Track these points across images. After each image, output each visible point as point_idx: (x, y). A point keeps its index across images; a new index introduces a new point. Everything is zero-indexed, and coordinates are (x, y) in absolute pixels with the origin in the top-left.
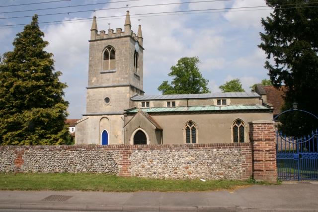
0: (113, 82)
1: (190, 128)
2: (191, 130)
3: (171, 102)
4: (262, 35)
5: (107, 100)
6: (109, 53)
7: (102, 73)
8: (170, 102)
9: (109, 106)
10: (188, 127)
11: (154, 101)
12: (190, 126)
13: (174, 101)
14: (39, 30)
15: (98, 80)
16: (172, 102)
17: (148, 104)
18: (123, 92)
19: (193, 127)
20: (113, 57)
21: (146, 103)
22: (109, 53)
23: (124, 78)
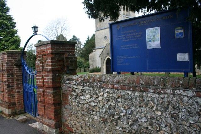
14: (77, 38)
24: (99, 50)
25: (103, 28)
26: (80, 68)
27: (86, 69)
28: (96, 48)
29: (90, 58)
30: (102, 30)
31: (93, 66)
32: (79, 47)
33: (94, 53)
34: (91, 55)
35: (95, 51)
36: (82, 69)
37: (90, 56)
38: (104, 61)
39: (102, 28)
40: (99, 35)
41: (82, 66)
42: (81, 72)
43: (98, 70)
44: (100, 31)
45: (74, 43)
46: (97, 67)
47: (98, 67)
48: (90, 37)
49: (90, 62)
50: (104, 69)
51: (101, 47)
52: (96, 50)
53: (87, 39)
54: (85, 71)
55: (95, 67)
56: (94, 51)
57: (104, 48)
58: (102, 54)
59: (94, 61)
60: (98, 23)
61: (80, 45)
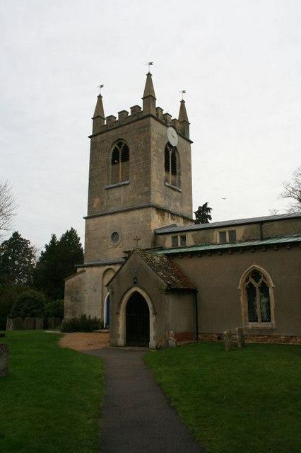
0: (125, 202)
1: (256, 285)
2: (258, 291)
3: (227, 230)
4: (54, 237)
5: (115, 235)
6: (120, 152)
7: (108, 189)
8: (225, 233)
9: (118, 248)
10: (251, 284)
11: (192, 233)
12: (257, 281)
13: (233, 229)
14: (22, 239)
15: (102, 203)
16: (230, 232)
17: (184, 238)
18: (141, 219)
19: (263, 283)
20: (126, 157)
21: (227, 234)
22: (120, 152)
23: (142, 194)
24: (94, 269)
25: (110, 211)
26: (34, 315)
27: (51, 320)
28: (85, 264)
29: (66, 289)
30: (106, 217)
31: (74, 313)
32: (25, 262)
33: (80, 276)
34: (69, 282)
35: (83, 271)
36: (39, 321)
37: (66, 283)
38: (120, 302)
39: (106, 212)
40: (95, 229)
41: (39, 310)
42: (35, 328)
43: (87, 326)
44: (102, 218)
45: (71, 236)
46: (84, 317)
47: (88, 317)
48: (58, 239)
49: (67, 301)
50: (119, 326)
51: (100, 263)
52: (85, 269)
53: (48, 242)
54: (46, 326)
55: (78, 316)
56: (79, 270)
57: (122, 264)
58: (115, 280)
59: (77, 300)
60: (94, 198)
61: (30, 258)
